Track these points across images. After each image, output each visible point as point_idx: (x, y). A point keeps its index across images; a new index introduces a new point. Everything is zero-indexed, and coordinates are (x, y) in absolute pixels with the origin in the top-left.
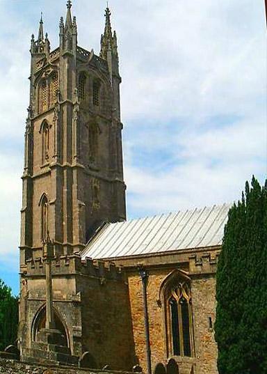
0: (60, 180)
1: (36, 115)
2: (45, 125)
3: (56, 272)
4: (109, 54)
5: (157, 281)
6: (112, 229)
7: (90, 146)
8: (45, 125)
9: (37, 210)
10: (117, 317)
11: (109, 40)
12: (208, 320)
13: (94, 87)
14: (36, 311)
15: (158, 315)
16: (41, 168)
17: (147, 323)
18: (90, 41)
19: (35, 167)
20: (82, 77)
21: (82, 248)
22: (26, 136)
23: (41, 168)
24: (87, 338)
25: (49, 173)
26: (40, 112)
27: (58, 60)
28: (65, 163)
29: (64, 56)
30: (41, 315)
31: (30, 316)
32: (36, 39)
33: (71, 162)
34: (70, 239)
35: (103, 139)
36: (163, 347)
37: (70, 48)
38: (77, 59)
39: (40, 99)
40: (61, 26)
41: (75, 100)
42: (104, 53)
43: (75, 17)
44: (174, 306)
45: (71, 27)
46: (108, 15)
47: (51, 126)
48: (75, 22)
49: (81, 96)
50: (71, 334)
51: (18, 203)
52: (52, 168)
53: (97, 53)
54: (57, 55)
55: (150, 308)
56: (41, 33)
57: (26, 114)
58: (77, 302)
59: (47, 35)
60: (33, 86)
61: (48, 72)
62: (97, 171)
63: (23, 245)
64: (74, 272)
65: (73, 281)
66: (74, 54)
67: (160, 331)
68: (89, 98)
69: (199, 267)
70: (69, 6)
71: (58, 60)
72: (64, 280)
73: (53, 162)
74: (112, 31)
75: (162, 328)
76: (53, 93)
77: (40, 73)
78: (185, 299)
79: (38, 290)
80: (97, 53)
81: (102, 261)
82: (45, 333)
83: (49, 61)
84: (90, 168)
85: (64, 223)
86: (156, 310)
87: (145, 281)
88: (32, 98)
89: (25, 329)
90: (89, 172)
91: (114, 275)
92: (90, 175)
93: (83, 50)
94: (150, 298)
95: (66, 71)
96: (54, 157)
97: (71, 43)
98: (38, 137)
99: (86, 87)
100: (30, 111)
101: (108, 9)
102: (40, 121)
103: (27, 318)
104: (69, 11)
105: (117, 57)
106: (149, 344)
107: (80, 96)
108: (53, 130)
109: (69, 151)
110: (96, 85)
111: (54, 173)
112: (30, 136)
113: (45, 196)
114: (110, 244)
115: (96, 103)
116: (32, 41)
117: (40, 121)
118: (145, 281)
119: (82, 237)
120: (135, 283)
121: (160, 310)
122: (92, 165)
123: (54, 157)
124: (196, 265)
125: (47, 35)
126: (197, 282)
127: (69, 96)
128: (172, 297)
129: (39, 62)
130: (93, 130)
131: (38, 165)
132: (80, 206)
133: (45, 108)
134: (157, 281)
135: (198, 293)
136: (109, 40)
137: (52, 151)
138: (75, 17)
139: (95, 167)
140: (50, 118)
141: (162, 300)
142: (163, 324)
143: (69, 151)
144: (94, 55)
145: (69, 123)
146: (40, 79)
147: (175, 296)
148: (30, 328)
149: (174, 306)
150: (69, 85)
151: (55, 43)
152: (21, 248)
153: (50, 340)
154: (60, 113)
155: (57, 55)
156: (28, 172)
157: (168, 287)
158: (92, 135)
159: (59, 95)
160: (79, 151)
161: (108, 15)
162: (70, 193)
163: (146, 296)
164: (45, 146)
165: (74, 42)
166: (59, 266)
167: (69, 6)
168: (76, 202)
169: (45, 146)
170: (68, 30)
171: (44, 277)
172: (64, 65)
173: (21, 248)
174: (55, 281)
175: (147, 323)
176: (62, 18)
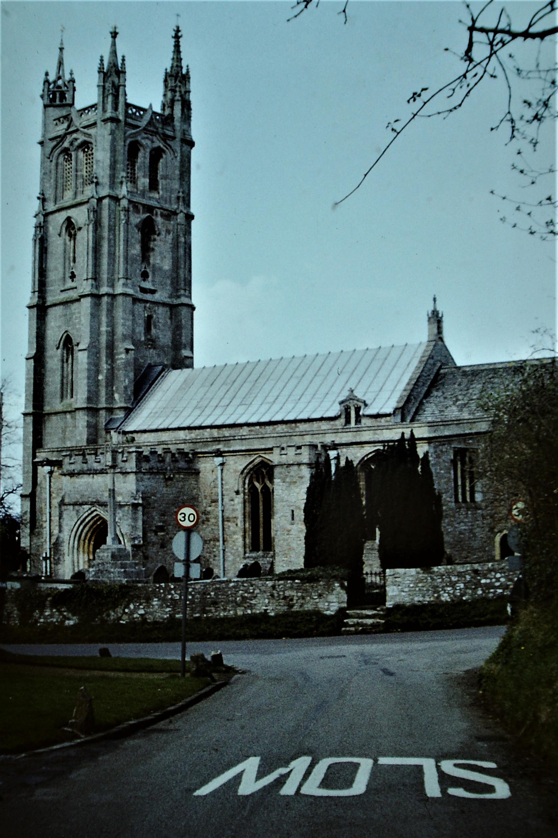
3: (56, 388)
9: (54, 357)
11: (177, 80)
12: (290, 513)
19: (50, 288)
21: (128, 411)
23: (62, 291)
28: (104, 290)
32: (52, 78)
34: (110, 397)
35: (162, 248)
37: (116, 108)
39: (60, 181)
42: (169, 104)
46: (177, 37)
48: (123, 64)
51: (24, 346)
53: (157, 109)
54: (92, 116)
60: (47, 157)
63: (31, 410)
65: (188, 644)
66: (121, 117)
75: (240, 522)
80: (157, 109)
90: (140, 296)
94: (227, 487)
98: (57, 243)
101: (178, 27)
102: (61, 217)
104: (114, 44)
107: (131, 171)
108: (85, 237)
109: (112, 272)
113: (68, 335)
114: (169, 410)
116: (46, 82)
117: (61, 217)
122: (147, 285)
127: (113, 184)
131: (57, 287)
140: (80, 216)
141: (241, 489)
143: (112, 272)
144: (154, 113)
146: (62, 149)
150: (113, 166)
151: (87, 94)
152: (25, 415)
154: (96, 212)
155: (92, 116)
156: (39, 297)
161: (177, 37)
163: (223, 479)
172: (102, 137)
173: (25, 415)
176: (102, 57)
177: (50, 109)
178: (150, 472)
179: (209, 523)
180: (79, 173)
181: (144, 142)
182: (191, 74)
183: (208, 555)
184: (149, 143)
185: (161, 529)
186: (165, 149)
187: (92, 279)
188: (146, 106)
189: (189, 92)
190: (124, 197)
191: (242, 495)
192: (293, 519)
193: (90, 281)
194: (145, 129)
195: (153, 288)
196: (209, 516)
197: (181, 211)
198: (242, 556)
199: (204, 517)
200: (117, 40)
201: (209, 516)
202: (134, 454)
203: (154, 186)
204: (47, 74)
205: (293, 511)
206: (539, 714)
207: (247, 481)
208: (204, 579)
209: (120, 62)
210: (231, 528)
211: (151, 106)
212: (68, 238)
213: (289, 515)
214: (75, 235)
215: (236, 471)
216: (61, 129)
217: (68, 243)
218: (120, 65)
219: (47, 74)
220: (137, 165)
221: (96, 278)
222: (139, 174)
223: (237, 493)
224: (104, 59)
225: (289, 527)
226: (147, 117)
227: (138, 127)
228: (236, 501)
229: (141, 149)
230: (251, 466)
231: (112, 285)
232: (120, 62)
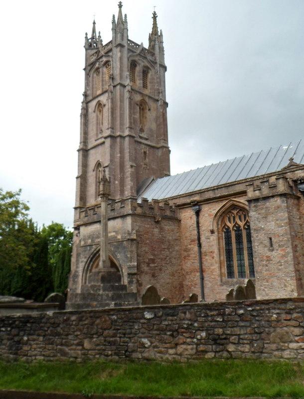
0: (112, 147)
1: (90, 98)
2: (100, 105)
4: (157, 47)
5: (210, 212)
6: (161, 182)
7: (140, 121)
8: (100, 105)
10: (170, 250)
11: (155, 36)
13: (143, 73)
14: (88, 256)
15: (212, 243)
16: (96, 140)
17: (200, 252)
18: (139, 35)
20: (133, 65)
22: (81, 116)
24: (142, 272)
25: (103, 143)
26: (94, 95)
27: (111, 50)
28: (118, 134)
29: (117, 46)
30: (95, 256)
31: (82, 262)
32: (90, 36)
33: (123, 132)
35: (151, 115)
36: (217, 272)
37: (122, 39)
38: (128, 49)
40: (114, 22)
41: (127, 82)
42: (152, 47)
43: (126, 15)
44: (228, 232)
45: (122, 22)
47: (104, 105)
49: (133, 80)
50: (125, 272)
51: (74, 170)
52: (106, 138)
55: (203, 238)
56: (94, 31)
57: (82, 98)
58: (132, 240)
59: (99, 33)
61: (101, 62)
62: (147, 139)
64: (130, 212)
65: (129, 220)
66: (126, 45)
67: (213, 258)
68: (139, 82)
69: (257, 192)
70: (120, 6)
71: (111, 50)
72: (119, 221)
73: (107, 133)
74: (159, 30)
75: (216, 255)
76: (107, 78)
77: (93, 64)
78: (229, 227)
79: (92, 237)
81: (156, 201)
82: (99, 272)
83: (102, 53)
84: (141, 137)
85: (117, 182)
86: (209, 239)
87: (198, 213)
88: (87, 84)
89: (76, 276)
90: (140, 140)
91: (166, 213)
92: (141, 143)
93: (133, 42)
95: (118, 59)
96: (108, 129)
97: (122, 36)
98: (92, 116)
99: (136, 74)
100: (85, 95)
101: (155, 12)
102: (94, 103)
103: (78, 265)
105: (163, 51)
106: (202, 271)
108: (106, 111)
109: (122, 124)
110: (145, 73)
111: (108, 141)
112: (85, 115)
114: (157, 191)
115: (145, 86)
116: (86, 37)
117: (94, 103)
118: (198, 213)
119: (133, 191)
120: (188, 216)
121: (214, 238)
122: (142, 135)
123: (108, 129)
124: (254, 191)
125: (99, 33)
126: (255, 206)
127: (121, 77)
128: (226, 225)
129: (93, 55)
130: (142, 106)
132: (132, 166)
133: (99, 92)
134: (210, 212)
135: (257, 216)
136: (155, 36)
137: (106, 124)
138: (126, 15)
139: (145, 136)
140: (104, 99)
141: (215, 229)
142: (216, 251)
145: (122, 101)
147: (228, 224)
148: (81, 274)
149: (228, 232)
150: (121, 70)
153: (103, 279)
157: (222, 215)
158: (141, 112)
159: (112, 78)
160: (130, 123)
162: (122, 158)
164: (99, 123)
165: (125, 35)
166: (114, 209)
167: (120, 6)
168: (128, 164)
169: (99, 123)
170: (120, 26)
171: (99, 222)
173: (75, 208)
174: (111, 224)
175: (200, 252)
177: (89, 51)
178: (143, 216)
179: (190, 258)
180: (104, 79)
181: (140, 62)
182: (163, 34)
183: (190, 283)
184: (142, 63)
185: (153, 261)
186: (150, 67)
187: (110, 128)
188: (140, 44)
189: (163, 43)
190: (128, 85)
191: (216, 233)
192: (271, 245)
193: (110, 130)
194: (139, 54)
195: (147, 137)
196: (189, 253)
197: (161, 99)
198: (219, 283)
199: (186, 254)
200: (122, 9)
201: (189, 253)
202: (130, 200)
203: (145, 86)
204: (86, 34)
205: (271, 239)
206: (47, 229)
207: (220, 223)
208: (192, 302)
209: (123, 16)
210: (209, 261)
211: (142, 44)
212: (99, 113)
213: (267, 242)
214: (103, 110)
215: (210, 215)
216: (93, 59)
217: (99, 115)
218: (124, 19)
219: (86, 34)
220: (136, 75)
221: (112, 128)
222: (137, 78)
223: (212, 232)
224: (115, 17)
225: (269, 254)
226: (141, 48)
227: (135, 52)
228: (212, 238)
229: (138, 65)
230: (223, 210)
231: (122, 130)
232: (123, 16)
